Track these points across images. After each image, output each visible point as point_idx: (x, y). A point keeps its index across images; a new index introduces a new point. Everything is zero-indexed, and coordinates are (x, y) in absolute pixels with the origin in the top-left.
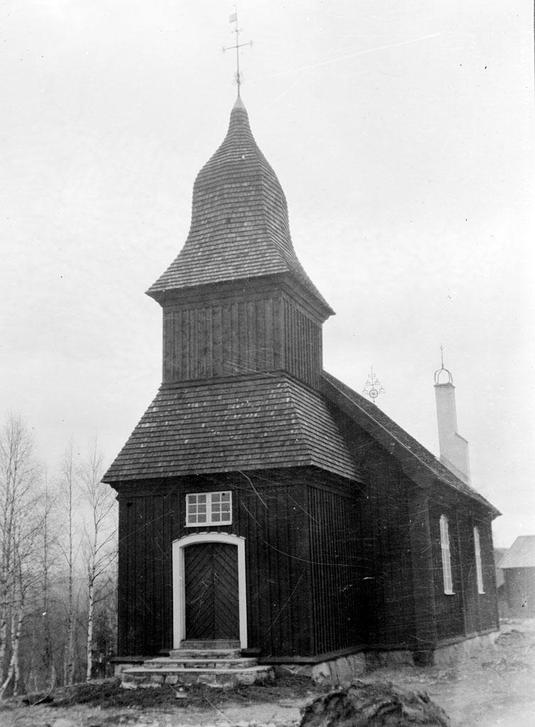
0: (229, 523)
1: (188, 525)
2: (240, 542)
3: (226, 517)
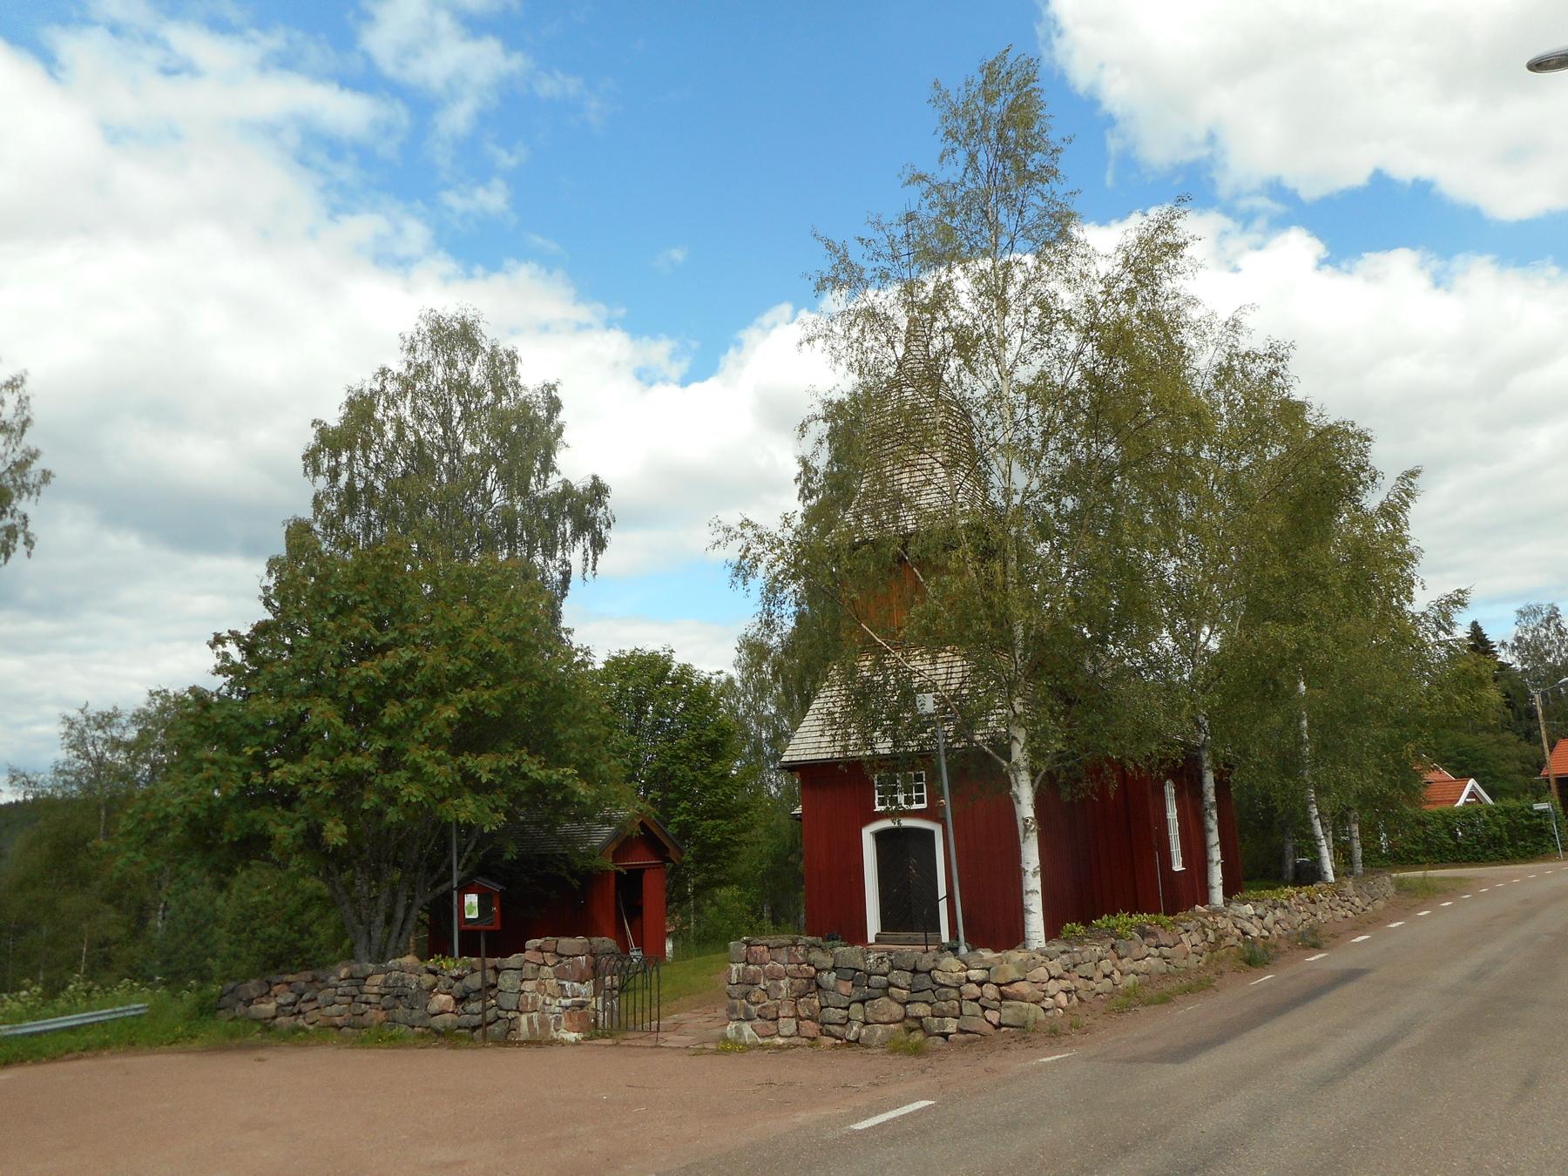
0: (924, 806)
1: (879, 808)
2: (938, 830)
3: (920, 800)
